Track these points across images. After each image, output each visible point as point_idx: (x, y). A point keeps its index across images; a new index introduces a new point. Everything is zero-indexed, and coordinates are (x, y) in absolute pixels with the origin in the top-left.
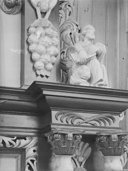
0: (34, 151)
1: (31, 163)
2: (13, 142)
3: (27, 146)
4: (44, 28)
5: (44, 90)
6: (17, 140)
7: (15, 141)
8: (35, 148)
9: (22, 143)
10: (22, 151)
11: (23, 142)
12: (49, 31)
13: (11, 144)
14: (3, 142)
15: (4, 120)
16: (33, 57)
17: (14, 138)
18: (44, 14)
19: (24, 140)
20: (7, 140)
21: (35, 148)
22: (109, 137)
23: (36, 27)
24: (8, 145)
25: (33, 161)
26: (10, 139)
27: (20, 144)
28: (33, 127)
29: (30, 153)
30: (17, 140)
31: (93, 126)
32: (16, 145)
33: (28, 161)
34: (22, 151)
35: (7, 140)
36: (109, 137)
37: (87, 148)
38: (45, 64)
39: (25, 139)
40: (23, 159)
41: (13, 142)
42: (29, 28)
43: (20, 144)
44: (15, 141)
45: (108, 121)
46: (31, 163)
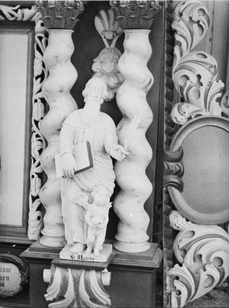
2: (14, 13)
6: (19, 10)
9: (25, 15)
11: (27, 13)
13: (12, 16)
15: (56, 200)
16: (212, 280)
17: (15, 6)
19: (84, 93)
20: (6, 10)
23: (114, 161)
27: (23, 16)
28: (126, 244)
30: (19, 10)
32: (19, 15)
35: (6, 10)
36: (176, 232)
39: (30, 8)
40: (34, 35)
41: (14, 13)
42: (111, 157)
43: (23, 16)
44: (16, 11)
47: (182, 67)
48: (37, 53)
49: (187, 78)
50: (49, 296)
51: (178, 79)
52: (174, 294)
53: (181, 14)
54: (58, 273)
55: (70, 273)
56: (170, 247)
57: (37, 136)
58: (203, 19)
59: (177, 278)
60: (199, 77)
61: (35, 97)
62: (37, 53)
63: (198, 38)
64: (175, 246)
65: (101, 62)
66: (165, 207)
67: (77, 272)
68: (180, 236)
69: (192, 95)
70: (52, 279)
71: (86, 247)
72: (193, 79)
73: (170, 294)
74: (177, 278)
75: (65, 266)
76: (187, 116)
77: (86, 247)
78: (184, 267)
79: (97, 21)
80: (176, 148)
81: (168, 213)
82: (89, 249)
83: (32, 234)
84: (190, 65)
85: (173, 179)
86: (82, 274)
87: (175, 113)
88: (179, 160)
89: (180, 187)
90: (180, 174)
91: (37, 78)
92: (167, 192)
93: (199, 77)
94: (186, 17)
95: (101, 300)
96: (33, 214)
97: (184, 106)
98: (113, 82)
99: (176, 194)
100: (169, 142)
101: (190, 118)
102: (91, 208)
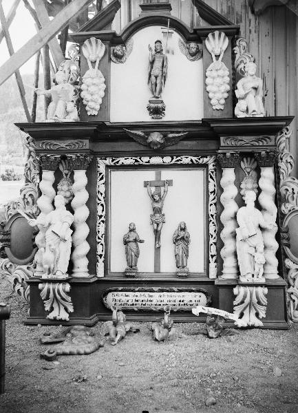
0: (213, 166)
1: (212, 174)
3: (198, 149)
4: (217, 70)
5: (202, 277)
7: (199, 159)
8: (213, 164)
10: (205, 166)
12: (220, 72)
14: (192, 160)
18: (217, 57)
21: (213, 164)
22: (36, 226)
24: (194, 162)
25: (212, 172)
26: (196, 158)
29: (211, 167)
31: (253, 145)
32: (200, 161)
33: (210, 172)
34: (205, 166)
36: (36, 226)
37: (254, 162)
38: (219, 101)
40: (207, 171)
44: (199, 159)
45: (266, 141)
46: (212, 174)
47: (284, 185)
48: (210, 179)
49: (287, 190)
50: (235, 303)
51: (282, 191)
52: (291, 302)
53: (281, 159)
54: (242, 289)
55: (248, 289)
56: (287, 278)
57: (213, 223)
58: (292, 161)
59: (292, 293)
60: (293, 189)
61: (210, 203)
62: (210, 179)
63: (290, 171)
64: (289, 277)
65: (246, 184)
66: (283, 257)
67: (251, 288)
68: (291, 272)
69: (290, 199)
70: (239, 293)
71: (253, 276)
72: (291, 191)
73: (289, 302)
74: (292, 293)
75: (245, 285)
76: (289, 209)
77: (253, 276)
78: (295, 288)
79: (242, 163)
80: (285, 226)
81: (284, 260)
82: (255, 276)
83: (213, 274)
84: (288, 183)
85: (285, 241)
86: (254, 289)
87: (283, 208)
88: (287, 232)
89: (289, 246)
90: (288, 239)
91: (211, 193)
92: (283, 249)
93: (293, 189)
94: (284, 160)
95: (263, 303)
96: (213, 265)
97: (287, 204)
98: (68, 194)
99: (288, 251)
100: (282, 223)
101: (290, 211)
102: (257, 255)
